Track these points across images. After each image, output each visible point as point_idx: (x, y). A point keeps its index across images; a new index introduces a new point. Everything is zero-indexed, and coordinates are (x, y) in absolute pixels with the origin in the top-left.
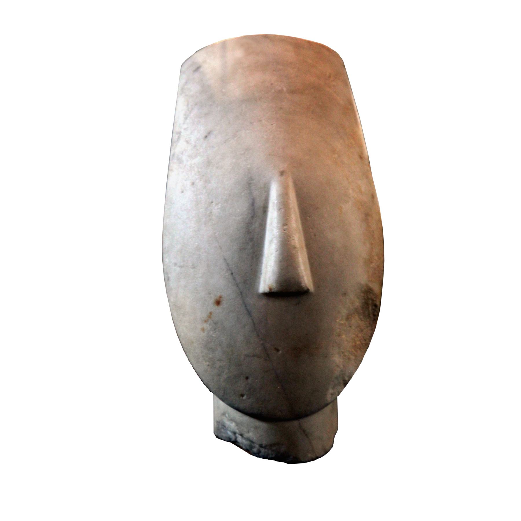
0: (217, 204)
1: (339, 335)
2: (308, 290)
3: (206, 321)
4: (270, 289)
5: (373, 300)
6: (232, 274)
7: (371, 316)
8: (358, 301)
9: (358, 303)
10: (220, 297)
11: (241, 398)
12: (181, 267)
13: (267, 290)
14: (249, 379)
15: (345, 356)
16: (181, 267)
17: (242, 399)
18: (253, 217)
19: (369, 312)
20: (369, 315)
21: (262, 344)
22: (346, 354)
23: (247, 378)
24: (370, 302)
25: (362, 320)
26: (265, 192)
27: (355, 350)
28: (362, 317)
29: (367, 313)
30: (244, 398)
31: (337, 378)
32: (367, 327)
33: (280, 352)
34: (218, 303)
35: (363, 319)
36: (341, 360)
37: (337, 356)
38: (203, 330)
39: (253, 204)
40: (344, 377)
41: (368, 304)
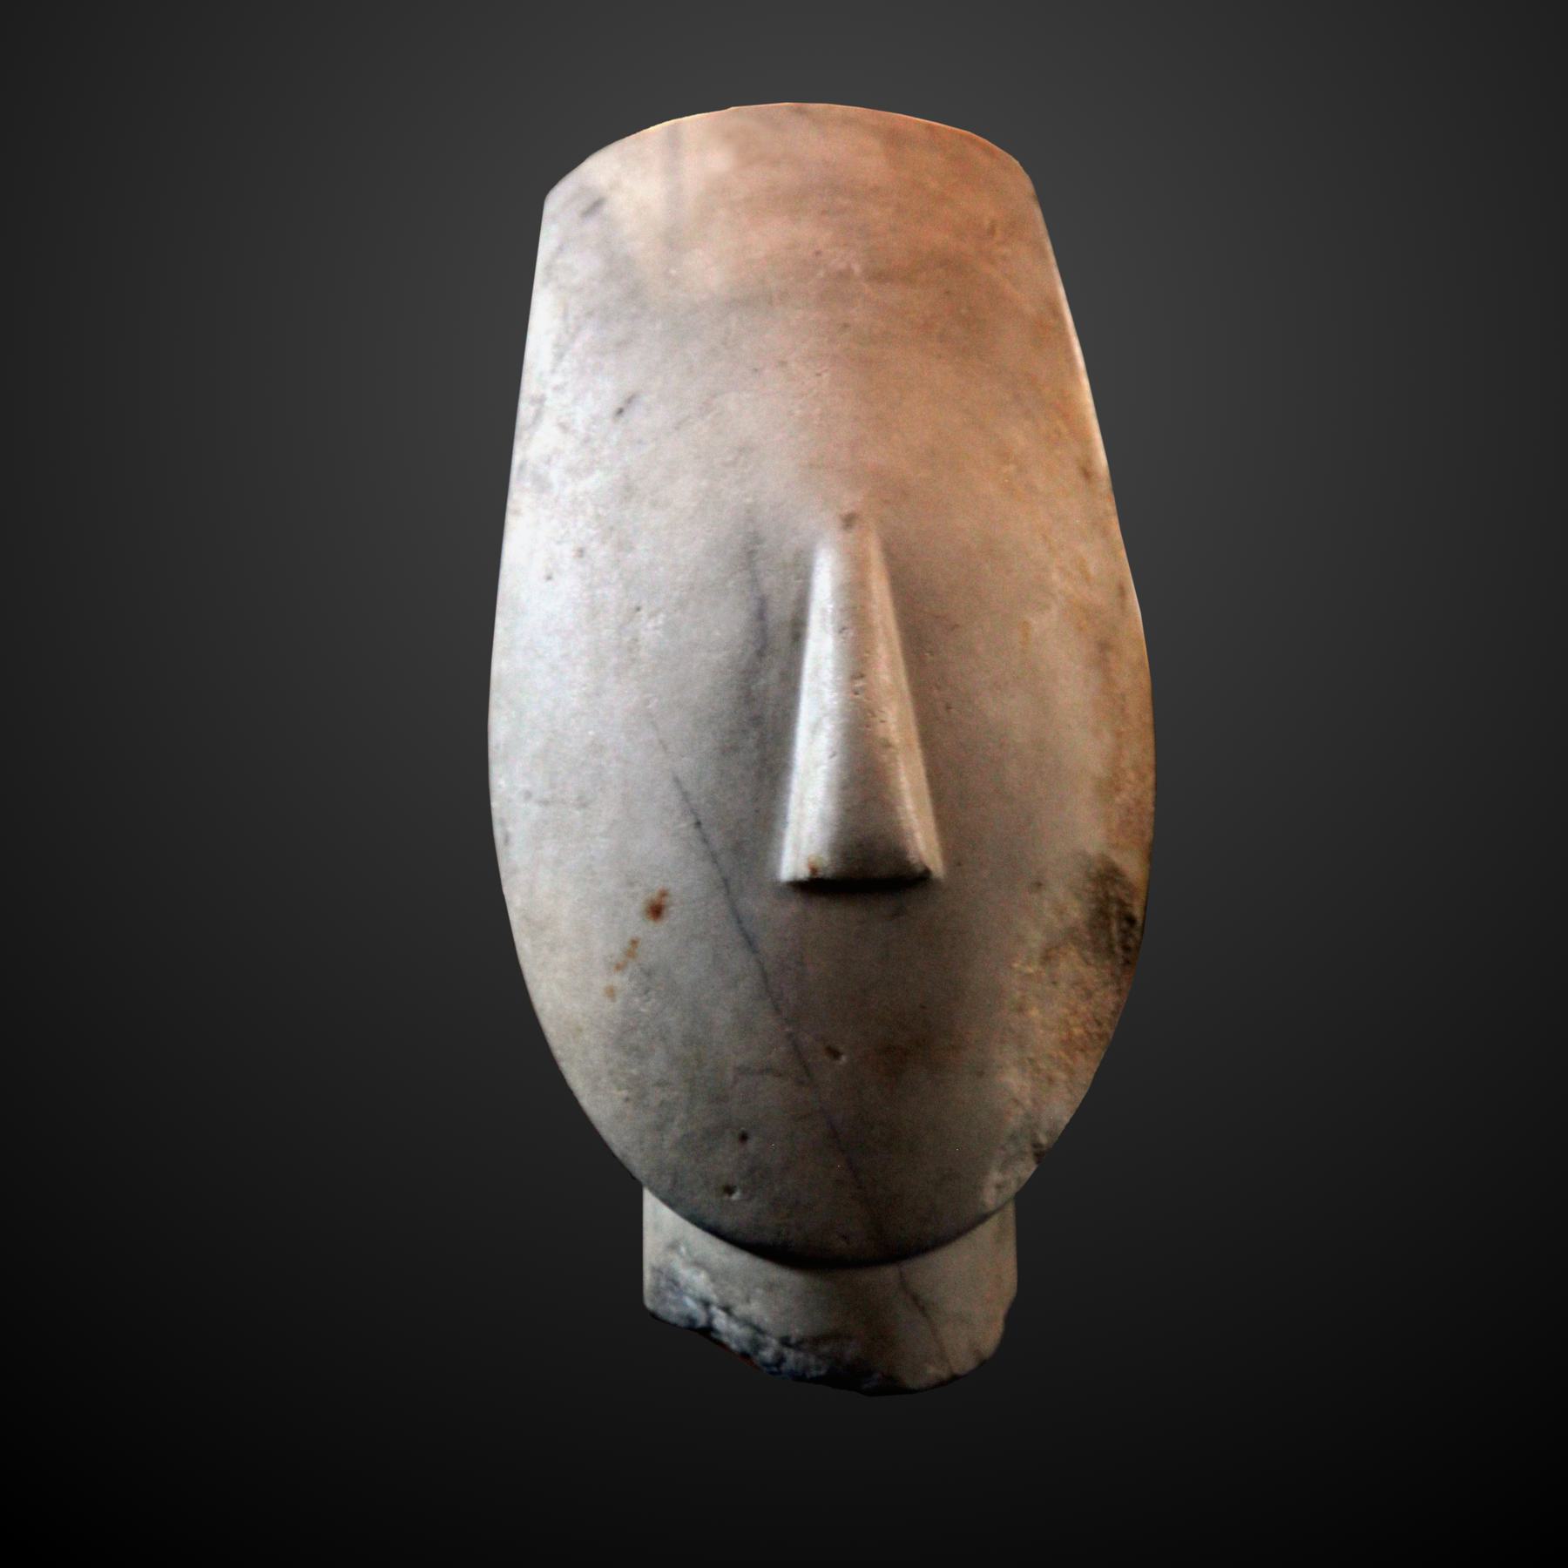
0: (653, 615)
1: (1021, 1009)
2: (927, 872)
3: (619, 967)
4: (814, 870)
5: (1121, 903)
6: (698, 824)
7: (1118, 950)
8: (1077, 904)
9: (1077, 912)
10: (664, 894)
11: (726, 1197)
12: (545, 803)
13: (803, 873)
14: (749, 1141)
15: (1038, 1070)
16: (545, 803)
17: (729, 1201)
18: (760, 654)
19: (1110, 938)
20: (1110, 947)
21: (790, 1035)
22: (1043, 1066)
23: (744, 1138)
24: (1114, 909)
25: (1088, 964)
26: (798, 578)
27: (1068, 1053)
28: (1088, 954)
29: (1103, 941)
30: (736, 1196)
31: (1013, 1138)
32: (1106, 984)
33: (844, 1059)
34: (656, 911)
35: (1092, 961)
36: (1028, 1084)
37: (1014, 1070)
38: (611, 993)
39: (761, 615)
40: (1035, 1135)
41: (1107, 916)
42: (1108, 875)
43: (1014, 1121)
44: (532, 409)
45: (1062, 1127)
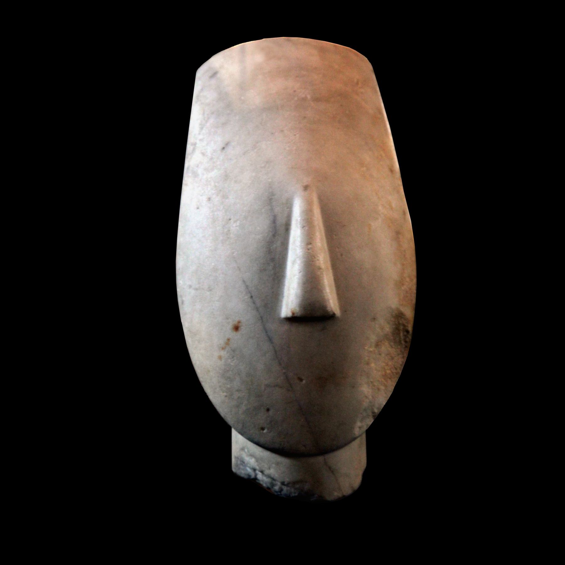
0: (235, 222)
1: (368, 364)
2: (334, 314)
4: (293, 314)
5: (404, 325)
6: (252, 297)
7: (403, 342)
8: (388, 326)
9: (388, 329)
10: (239, 322)
11: (262, 431)
12: (196, 289)
13: (289, 315)
14: (270, 411)
15: (374, 386)
16: (196, 289)
17: (263, 433)
18: (274, 236)
19: (400, 338)
20: (400, 341)
21: (285, 373)
22: (376, 384)
23: (268, 410)
24: (401, 327)
25: (392, 347)
26: (288, 208)
27: (385, 379)
28: (392, 344)
29: (397, 339)
30: (265, 431)
31: (365, 410)
32: (398, 355)
33: (304, 381)
34: (236, 328)
35: (394, 346)
36: (370, 391)
37: (365, 386)
38: (220, 358)
39: (274, 221)
40: (373, 409)
41: (399, 330)
42: (399, 315)
43: (365, 404)
44: (192, 147)
45: (409, 313)
